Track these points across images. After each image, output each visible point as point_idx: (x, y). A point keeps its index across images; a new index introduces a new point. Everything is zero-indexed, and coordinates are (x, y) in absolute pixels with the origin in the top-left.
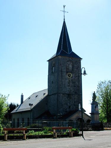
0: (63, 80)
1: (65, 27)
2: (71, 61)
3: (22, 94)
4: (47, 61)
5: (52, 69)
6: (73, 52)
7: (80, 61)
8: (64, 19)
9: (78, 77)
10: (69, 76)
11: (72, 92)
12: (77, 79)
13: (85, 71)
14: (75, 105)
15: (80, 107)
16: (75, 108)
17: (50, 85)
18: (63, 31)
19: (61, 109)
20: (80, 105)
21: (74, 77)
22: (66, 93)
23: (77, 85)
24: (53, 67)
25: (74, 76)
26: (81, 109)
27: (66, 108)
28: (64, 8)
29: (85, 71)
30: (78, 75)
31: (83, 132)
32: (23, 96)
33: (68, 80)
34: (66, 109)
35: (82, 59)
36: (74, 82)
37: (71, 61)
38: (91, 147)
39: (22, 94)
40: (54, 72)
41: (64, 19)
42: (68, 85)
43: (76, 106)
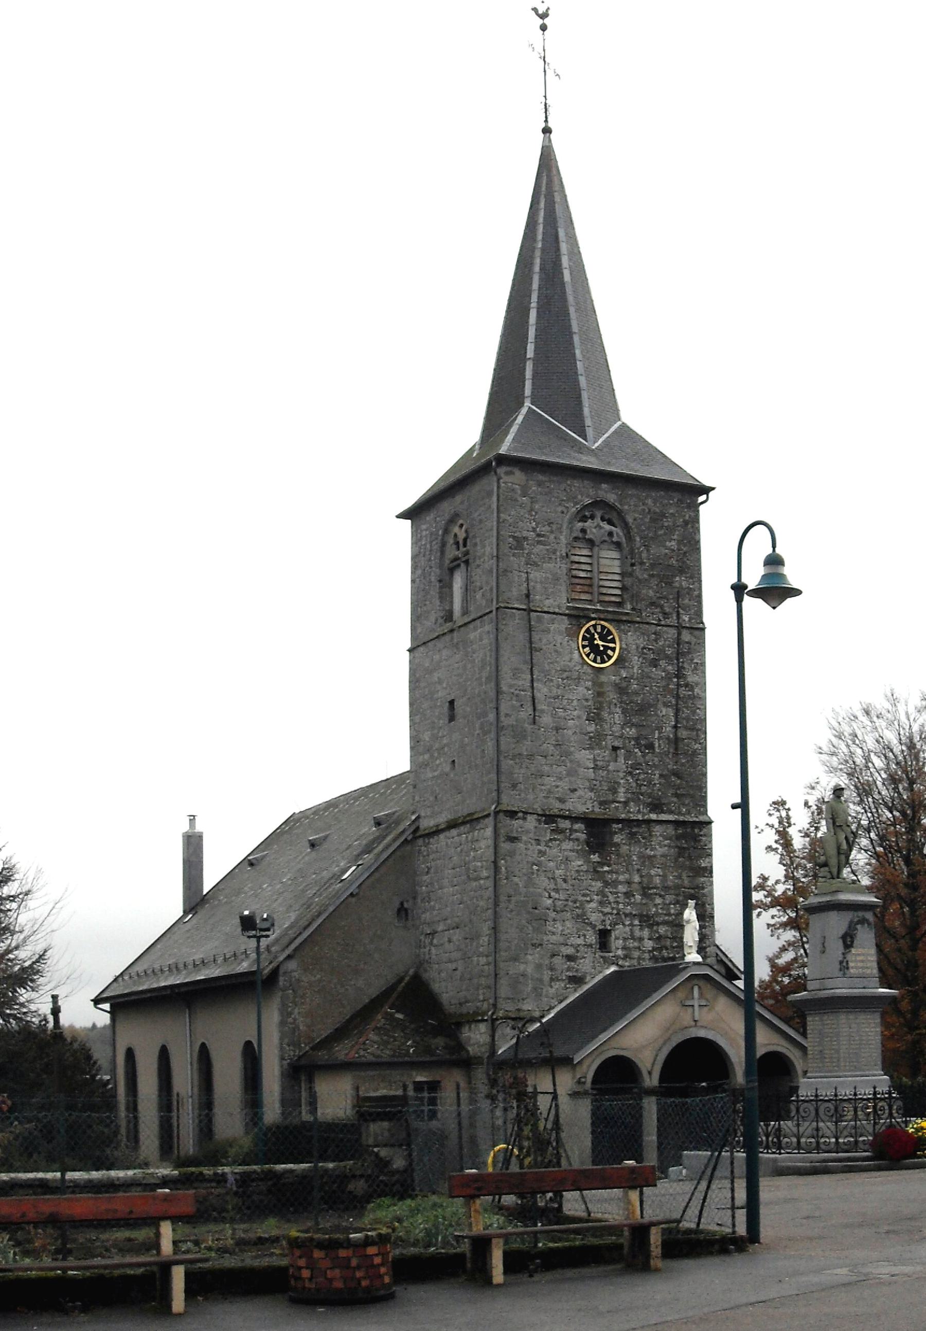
0: (542, 691)
1: (557, 198)
2: (614, 516)
3: (192, 819)
4: (404, 515)
5: (445, 585)
6: (626, 433)
7: (695, 507)
8: (547, 131)
9: (679, 654)
10: (594, 649)
11: (621, 797)
12: (668, 678)
13: (774, 561)
14: (647, 920)
15: (691, 935)
16: (649, 944)
17: (426, 736)
18: (540, 228)
19: (533, 957)
20: (690, 914)
21: (636, 660)
22: (568, 806)
23: (668, 730)
24: (452, 571)
25: (642, 652)
26: (701, 950)
27: (570, 951)
28: (544, 28)
29: (774, 561)
30: (678, 641)
31: (538, 1091)
32: (200, 837)
33: (583, 691)
34: (570, 958)
35: (706, 490)
36: (643, 709)
37: (614, 516)
38: (492, 1118)
39: (192, 819)
40: (465, 612)
41: (547, 131)
42: (592, 728)
43: (662, 930)
